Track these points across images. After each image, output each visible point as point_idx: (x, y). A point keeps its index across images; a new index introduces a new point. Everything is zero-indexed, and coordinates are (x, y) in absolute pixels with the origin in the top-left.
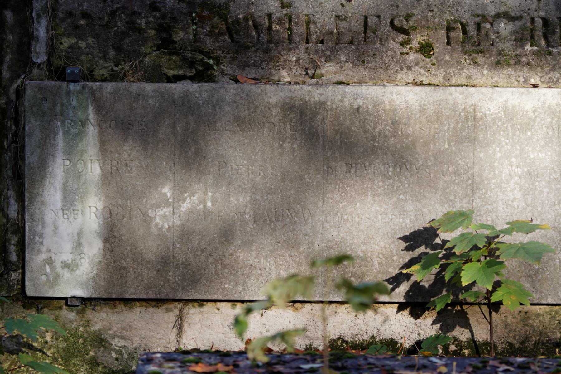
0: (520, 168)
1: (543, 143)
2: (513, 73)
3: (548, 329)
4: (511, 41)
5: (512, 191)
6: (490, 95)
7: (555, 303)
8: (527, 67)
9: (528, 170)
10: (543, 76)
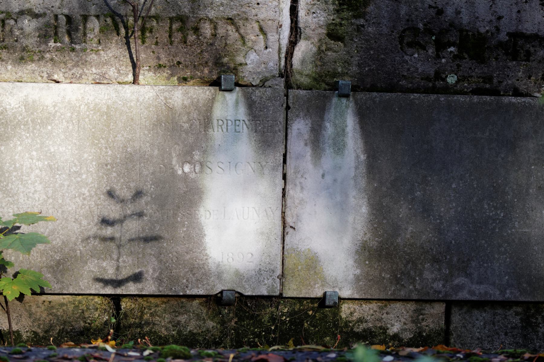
0: (41, 161)
1: (63, 137)
2: (36, 68)
3: (72, 318)
4: (35, 37)
5: (33, 183)
6: (10, 90)
7: (76, 293)
8: (50, 63)
9: (49, 163)
10: (66, 72)
